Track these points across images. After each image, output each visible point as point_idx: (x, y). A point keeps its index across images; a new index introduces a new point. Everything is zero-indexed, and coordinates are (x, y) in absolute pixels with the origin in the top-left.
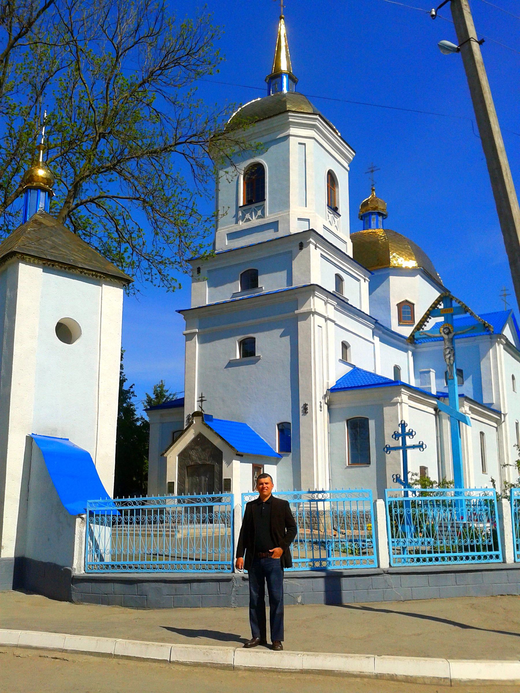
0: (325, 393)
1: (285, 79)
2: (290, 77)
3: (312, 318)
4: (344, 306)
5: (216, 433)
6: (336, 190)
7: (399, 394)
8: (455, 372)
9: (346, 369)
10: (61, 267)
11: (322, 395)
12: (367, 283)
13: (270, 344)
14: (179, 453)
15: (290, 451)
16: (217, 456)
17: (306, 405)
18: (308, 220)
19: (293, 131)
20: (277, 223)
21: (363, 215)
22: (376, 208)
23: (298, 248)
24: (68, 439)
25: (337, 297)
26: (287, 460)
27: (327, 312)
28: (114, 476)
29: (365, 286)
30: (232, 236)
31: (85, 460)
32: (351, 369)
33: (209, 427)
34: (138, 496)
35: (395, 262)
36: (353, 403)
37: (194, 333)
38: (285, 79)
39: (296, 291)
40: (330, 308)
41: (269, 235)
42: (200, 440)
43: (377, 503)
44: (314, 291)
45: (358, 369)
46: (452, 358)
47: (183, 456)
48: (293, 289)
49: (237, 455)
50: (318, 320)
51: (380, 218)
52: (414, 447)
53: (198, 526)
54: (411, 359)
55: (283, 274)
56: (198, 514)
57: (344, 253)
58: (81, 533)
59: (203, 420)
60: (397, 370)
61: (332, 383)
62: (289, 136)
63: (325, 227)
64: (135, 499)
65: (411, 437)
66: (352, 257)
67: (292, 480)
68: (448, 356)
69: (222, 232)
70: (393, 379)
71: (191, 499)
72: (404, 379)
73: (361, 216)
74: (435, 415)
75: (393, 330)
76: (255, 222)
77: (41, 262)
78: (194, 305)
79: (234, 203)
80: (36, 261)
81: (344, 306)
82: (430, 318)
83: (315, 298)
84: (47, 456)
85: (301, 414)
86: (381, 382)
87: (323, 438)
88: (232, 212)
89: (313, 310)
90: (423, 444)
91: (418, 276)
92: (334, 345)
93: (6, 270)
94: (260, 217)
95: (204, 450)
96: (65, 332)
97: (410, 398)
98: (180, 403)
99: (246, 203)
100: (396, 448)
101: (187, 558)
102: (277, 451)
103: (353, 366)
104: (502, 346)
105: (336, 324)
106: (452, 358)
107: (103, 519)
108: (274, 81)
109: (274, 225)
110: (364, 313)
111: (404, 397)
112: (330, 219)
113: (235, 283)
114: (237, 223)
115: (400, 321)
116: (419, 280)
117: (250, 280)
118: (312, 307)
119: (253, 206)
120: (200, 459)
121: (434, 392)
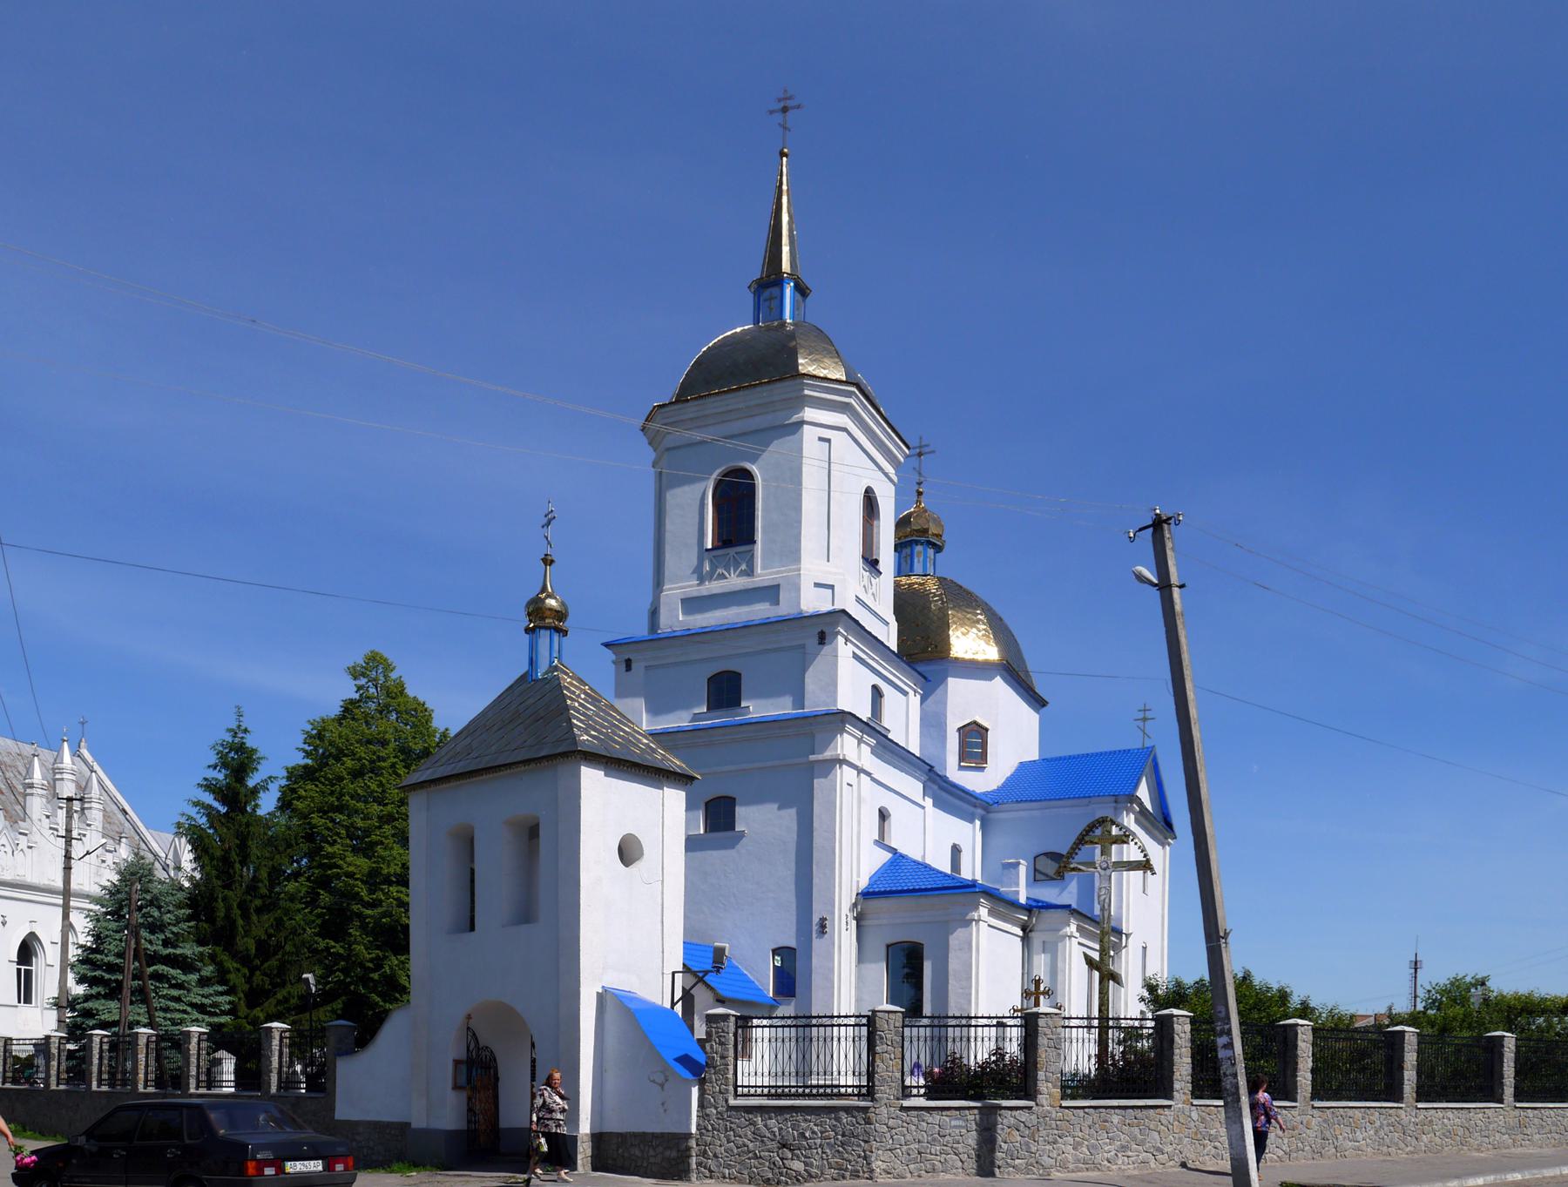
8: (1053, 866)
15: (793, 995)
17: (823, 920)
18: (832, 587)
19: (810, 414)
20: (777, 587)
22: (925, 531)
25: (872, 729)
30: (692, 604)
40: (866, 750)
41: (760, 611)
44: (843, 722)
45: (903, 856)
50: (847, 774)
61: (864, 883)
62: (802, 423)
63: (858, 600)
66: (895, 649)
69: (679, 586)
76: (735, 582)
79: (695, 541)
88: (692, 558)
91: (998, 679)
94: (742, 573)
97: (991, 913)
103: (894, 851)
104: (1132, 816)
105: (874, 780)
108: (766, 293)
109: (771, 593)
112: (866, 582)
115: (961, 760)
116: (999, 687)
117: (725, 691)
119: (732, 551)
121: (1023, 900)
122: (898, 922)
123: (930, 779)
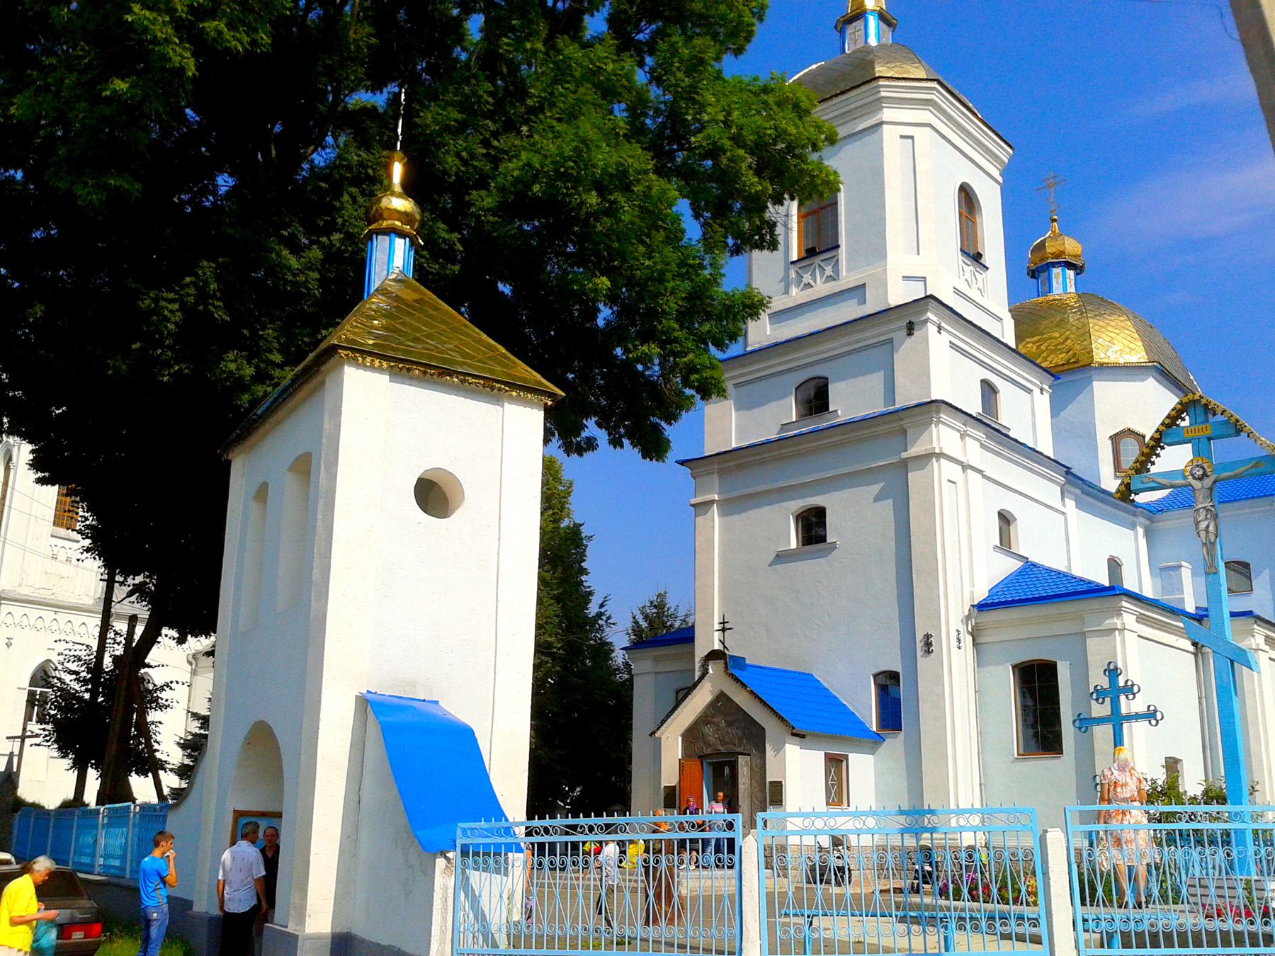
0: (966, 613)
1: (872, 22)
2: (882, 17)
3: (936, 465)
4: (999, 437)
5: (752, 692)
6: (978, 220)
7: (1118, 612)
9: (1006, 566)
10: (425, 373)
11: (961, 617)
12: (1046, 396)
13: (854, 514)
14: (683, 730)
16: (755, 738)
17: (928, 636)
18: (924, 279)
19: (888, 114)
21: (1034, 268)
23: (905, 332)
24: (437, 702)
25: (987, 424)
26: (894, 744)
27: (965, 454)
28: (527, 774)
29: (1043, 401)
31: (459, 744)
32: (1021, 564)
33: (737, 680)
34: (599, 815)
35: (1102, 355)
36: (1030, 635)
37: (712, 502)
38: (872, 22)
39: (901, 414)
40: (973, 445)
42: (721, 703)
43: (1049, 835)
44: (938, 412)
45: (1034, 565)
46: (1211, 528)
47: (691, 735)
48: (897, 411)
49: (793, 734)
51: (1071, 273)
52: (1137, 717)
53: (719, 873)
54: (1143, 542)
55: (875, 381)
56: (670, 856)
57: (998, 340)
58: (445, 889)
59: (726, 668)
60: (1114, 566)
61: (981, 594)
62: (881, 124)
63: (957, 292)
64: (593, 820)
65: (1131, 697)
67: (906, 784)
68: (1203, 525)
70: (1107, 584)
71: (567, 826)
72: (1129, 584)
73: (1033, 272)
74: (1196, 655)
75: (1103, 486)
76: (822, 287)
77: (385, 364)
78: (710, 449)
80: (377, 362)
81: (999, 437)
82: (1163, 448)
83: (941, 426)
84: (388, 732)
85: (919, 653)
86: (1079, 588)
87: (967, 701)
89: (937, 451)
90: (1155, 711)
92: (983, 515)
93: (322, 384)
94: (831, 278)
95: (729, 724)
96: (433, 495)
97: (1141, 619)
98: (686, 636)
99: (803, 254)
100: (1101, 721)
101: (673, 945)
102: (874, 729)
105: (984, 477)
106: (1211, 528)
107: (486, 863)
108: (850, 29)
109: (859, 290)
110: (1041, 454)
111: (1129, 620)
112: (968, 276)
113: (782, 402)
114: (787, 292)
117: (816, 399)
118: (935, 444)
119: (817, 260)
120: (723, 743)
121: (1190, 608)
122: (1030, 635)
123: (1068, 482)
